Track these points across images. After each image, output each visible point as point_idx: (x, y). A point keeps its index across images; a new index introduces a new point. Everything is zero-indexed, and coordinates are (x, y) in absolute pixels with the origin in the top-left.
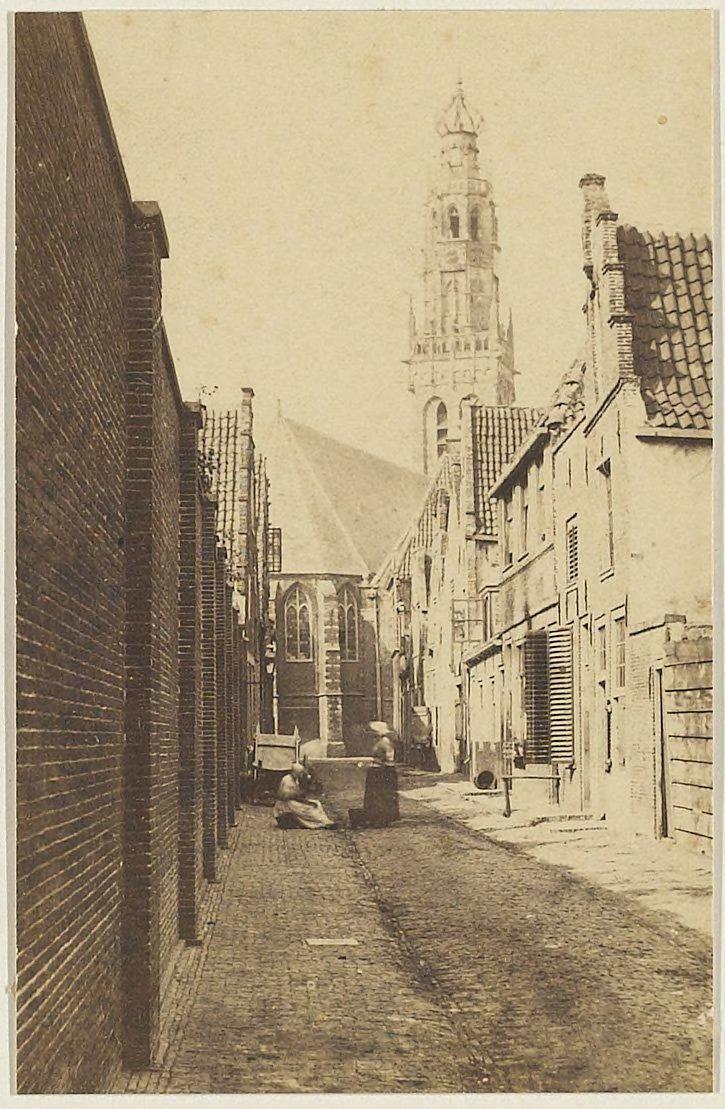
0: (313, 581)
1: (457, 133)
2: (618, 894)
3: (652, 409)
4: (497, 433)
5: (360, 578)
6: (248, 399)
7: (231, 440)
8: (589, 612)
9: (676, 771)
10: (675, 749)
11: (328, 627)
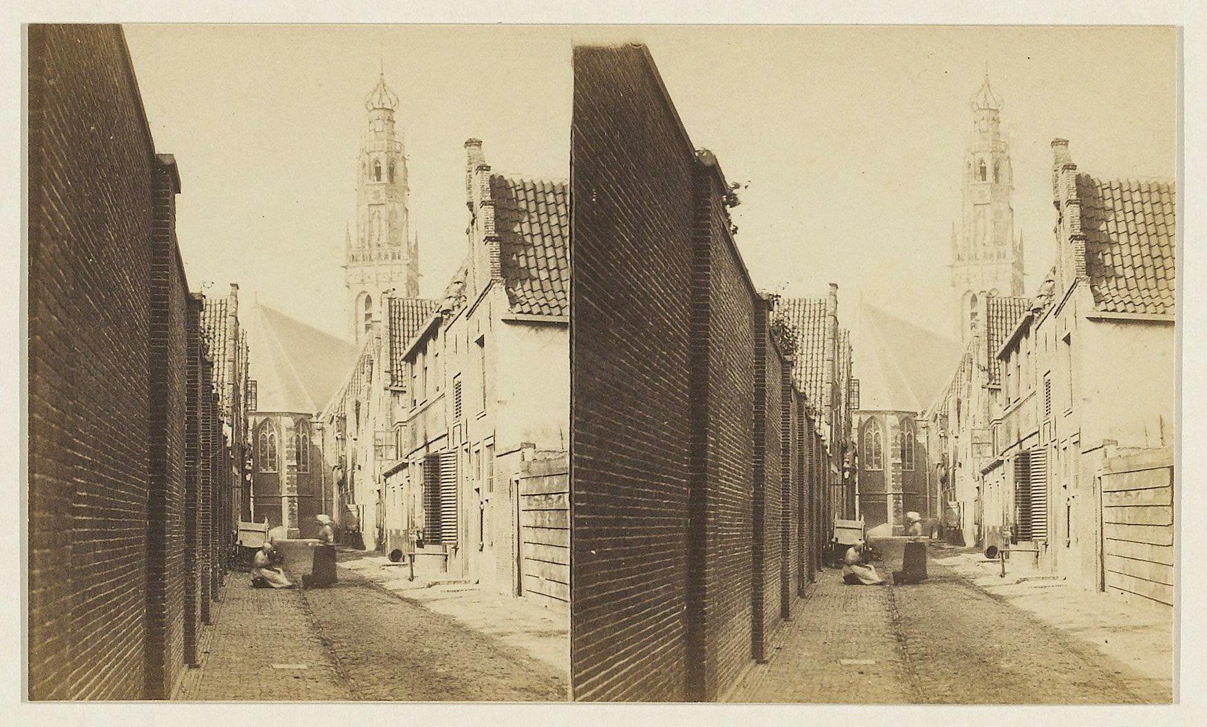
7: (822, 319)
9: (1109, 546)
10: (1109, 531)
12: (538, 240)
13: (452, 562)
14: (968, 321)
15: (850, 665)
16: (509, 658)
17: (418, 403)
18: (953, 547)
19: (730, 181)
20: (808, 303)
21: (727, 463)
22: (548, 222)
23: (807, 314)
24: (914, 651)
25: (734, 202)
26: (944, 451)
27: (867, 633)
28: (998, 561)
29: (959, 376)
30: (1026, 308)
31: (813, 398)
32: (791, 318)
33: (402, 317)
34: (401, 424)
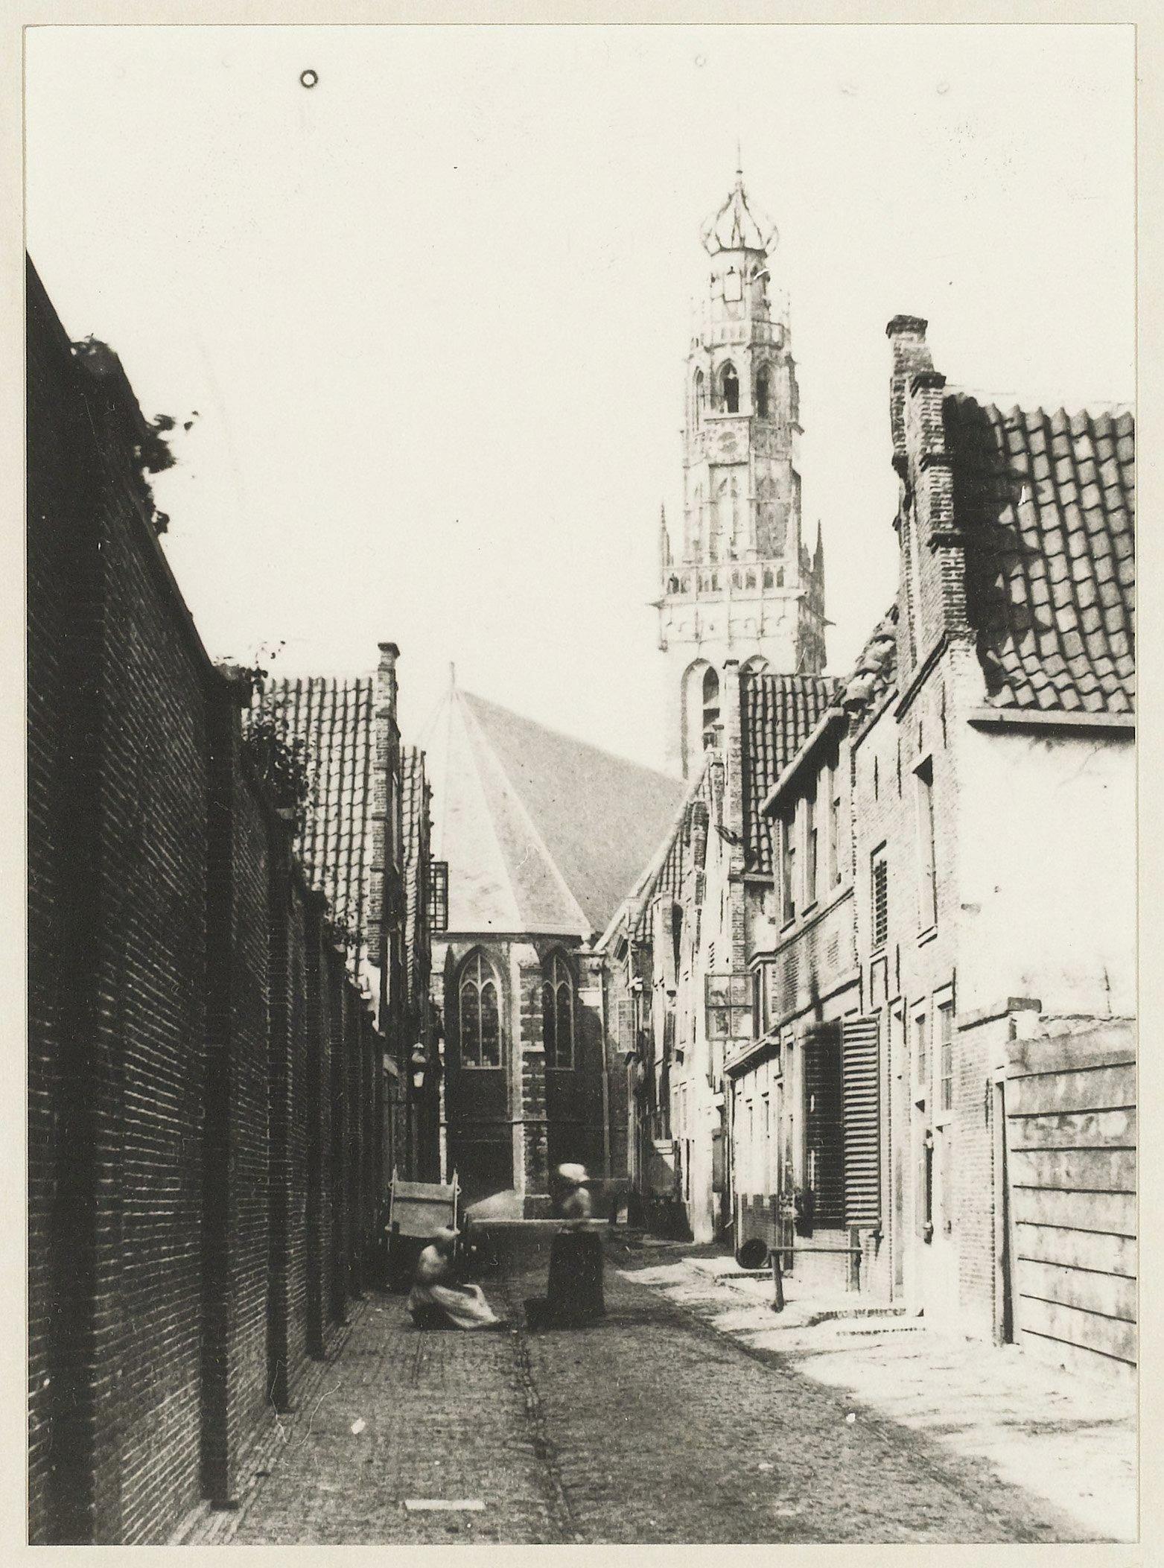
0: (504, 946)
1: (737, 249)
2: (915, 1432)
3: (995, 678)
4: (779, 717)
5: (576, 941)
6: (388, 661)
7: (362, 725)
8: (902, 993)
9: (1023, 1240)
10: (1023, 1205)
11: (528, 1016)
12: (1053, 543)
13: (870, 1266)
14: (697, 729)
15: (426, 1513)
16: (950, 1480)
17: (799, 909)
18: (663, 1243)
19: (150, 413)
20: (329, 687)
21: (142, 1052)
22: (1078, 502)
23: (327, 714)
24: (576, 1479)
25: (162, 459)
26: (643, 1024)
27: (466, 1440)
28: (769, 1275)
29: (678, 854)
30: (830, 700)
31: (340, 904)
32: (291, 724)
33: (770, 716)
34: (766, 958)
